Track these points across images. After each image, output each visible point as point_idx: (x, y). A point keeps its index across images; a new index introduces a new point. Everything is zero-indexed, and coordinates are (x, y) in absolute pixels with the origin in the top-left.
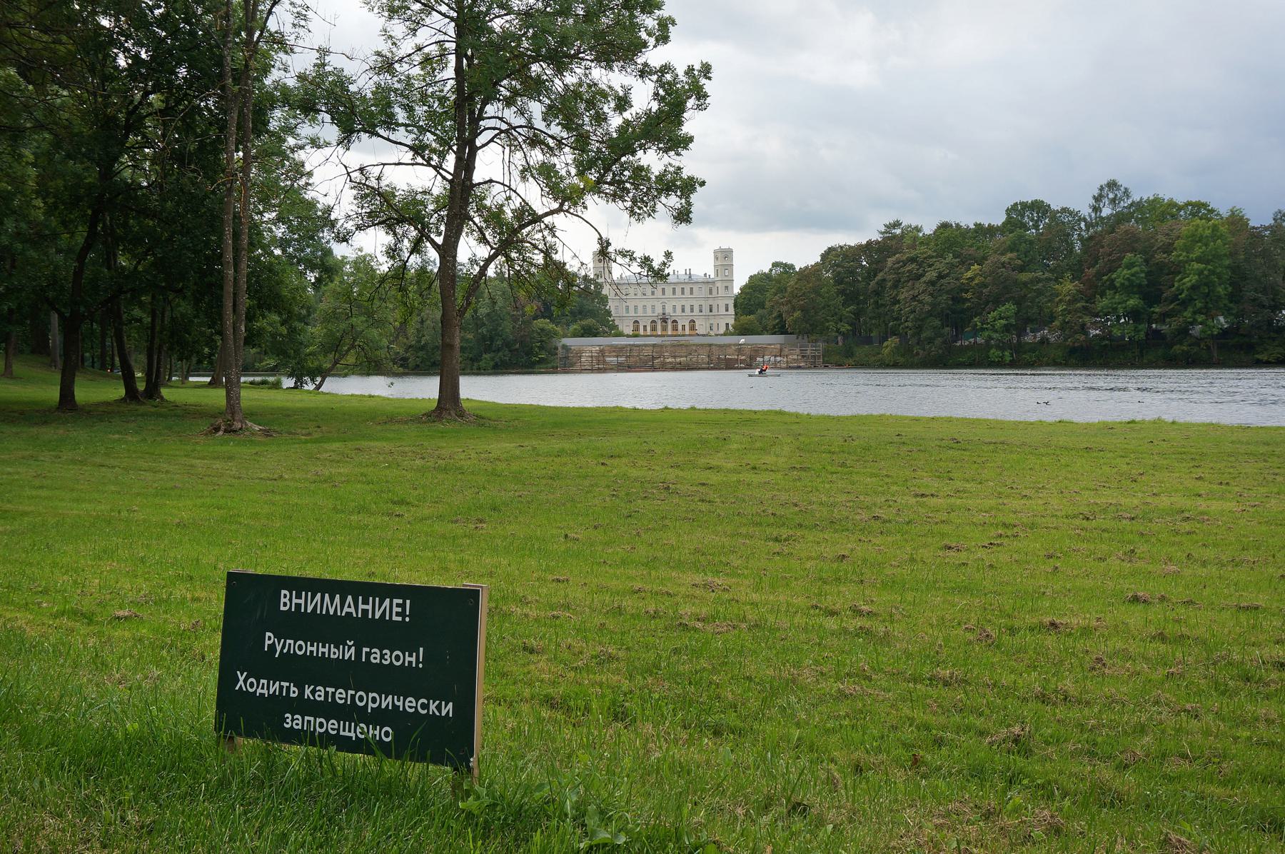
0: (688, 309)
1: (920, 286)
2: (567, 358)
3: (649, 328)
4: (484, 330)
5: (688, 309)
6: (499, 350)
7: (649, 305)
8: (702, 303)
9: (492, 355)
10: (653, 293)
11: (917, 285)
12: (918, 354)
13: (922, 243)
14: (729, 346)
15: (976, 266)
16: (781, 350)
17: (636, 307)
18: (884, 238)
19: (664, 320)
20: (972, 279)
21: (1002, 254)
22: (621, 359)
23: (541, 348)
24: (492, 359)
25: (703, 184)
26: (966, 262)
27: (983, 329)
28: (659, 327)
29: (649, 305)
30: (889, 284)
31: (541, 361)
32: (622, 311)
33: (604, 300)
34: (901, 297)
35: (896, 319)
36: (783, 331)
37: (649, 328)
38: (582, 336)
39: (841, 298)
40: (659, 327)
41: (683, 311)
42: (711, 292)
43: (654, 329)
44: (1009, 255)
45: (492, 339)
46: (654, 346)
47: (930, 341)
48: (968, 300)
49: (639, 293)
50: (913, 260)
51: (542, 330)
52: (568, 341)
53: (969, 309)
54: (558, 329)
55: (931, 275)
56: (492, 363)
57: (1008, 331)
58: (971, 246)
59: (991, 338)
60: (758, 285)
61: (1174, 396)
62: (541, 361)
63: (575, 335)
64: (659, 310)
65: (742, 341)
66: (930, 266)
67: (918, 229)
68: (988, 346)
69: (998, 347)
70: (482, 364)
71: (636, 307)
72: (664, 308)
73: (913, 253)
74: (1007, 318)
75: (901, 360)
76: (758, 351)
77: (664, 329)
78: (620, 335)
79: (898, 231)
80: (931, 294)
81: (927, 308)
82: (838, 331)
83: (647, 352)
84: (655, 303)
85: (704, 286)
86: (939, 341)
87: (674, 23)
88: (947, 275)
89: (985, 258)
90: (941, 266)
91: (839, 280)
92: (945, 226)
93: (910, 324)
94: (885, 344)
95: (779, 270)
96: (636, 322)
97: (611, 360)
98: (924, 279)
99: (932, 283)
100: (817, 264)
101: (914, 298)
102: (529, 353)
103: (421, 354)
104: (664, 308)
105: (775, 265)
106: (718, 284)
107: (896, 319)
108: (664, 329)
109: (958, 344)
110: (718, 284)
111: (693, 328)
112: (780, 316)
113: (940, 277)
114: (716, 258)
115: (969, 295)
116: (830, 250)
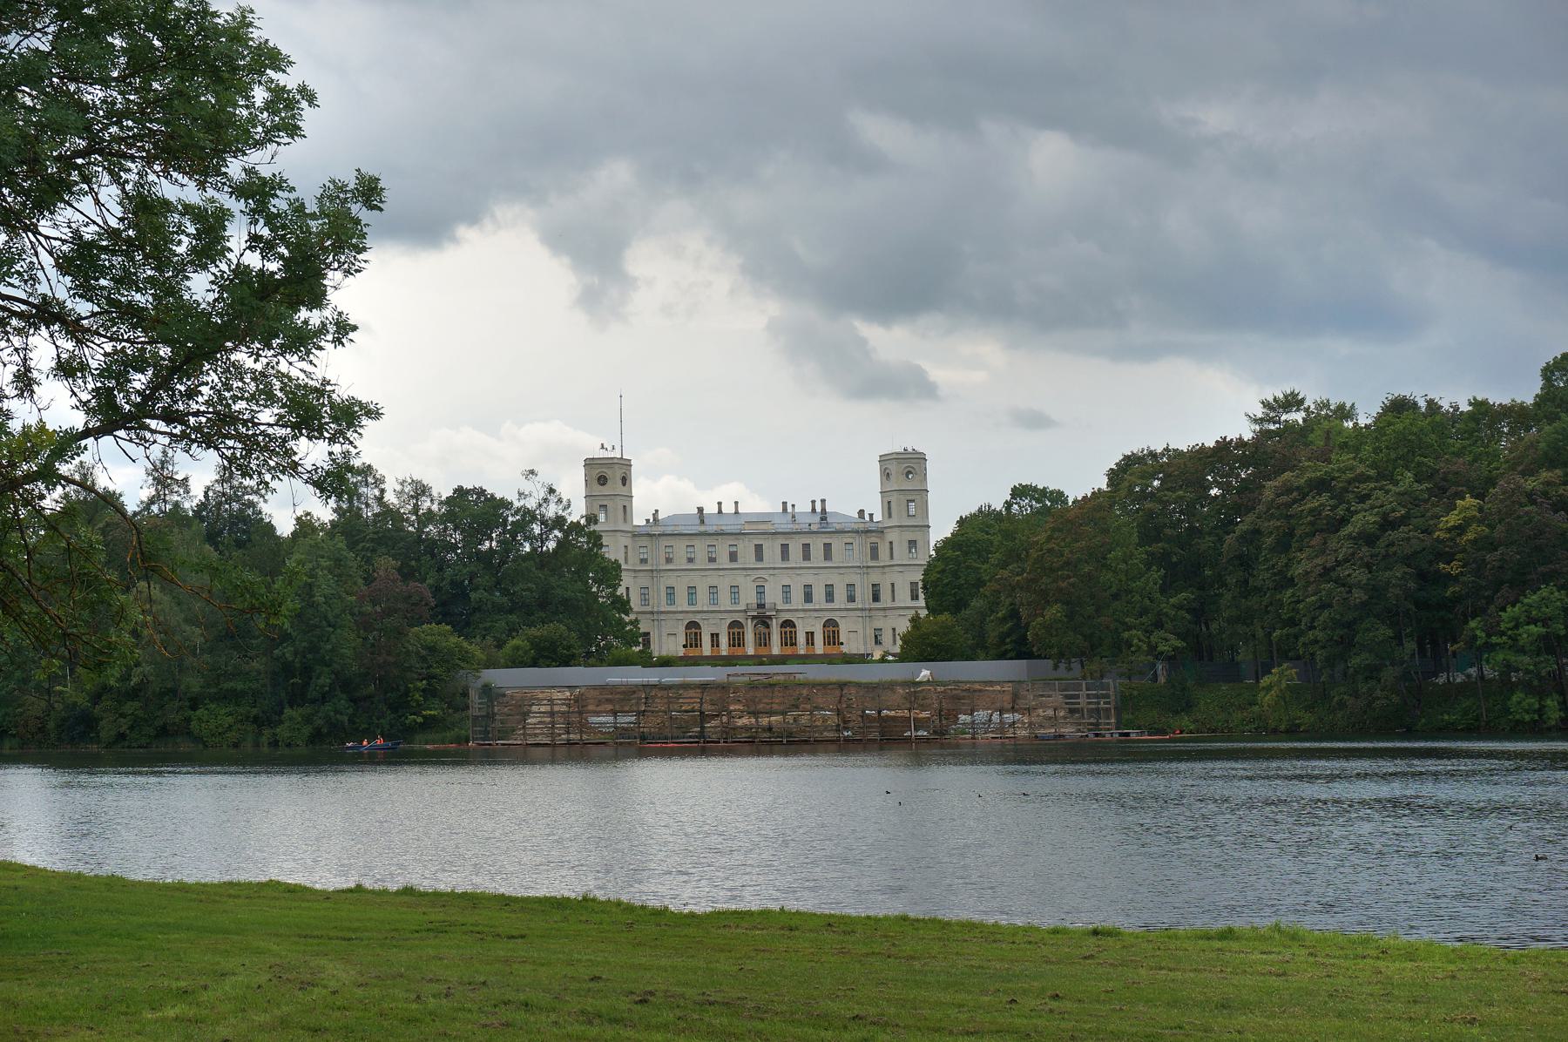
0: (819, 594)
1: (1340, 546)
2: (490, 716)
3: (724, 640)
4: (287, 651)
5: (819, 594)
6: (324, 698)
7: (724, 585)
8: (854, 578)
9: (307, 709)
10: (733, 557)
11: (1333, 544)
12: (1342, 705)
13: (1344, 446)
14: (891, 686)
15: (1469, 501)
16: (1015, 697)
17: (692, 590)
18: (1264, 435)
19: (763, 621)
20: (1460, 529)
21: (1529, 472)
22: (626, 720)
23: (429, 693)
24: (308, 720)
25: (374, 413)
26: (1445, 490)
27: (1490, 647)
28: (749, 637)
29: (724, 585)
30: (1269, 541)
31: (429, 724)
32: (663, 607)
33: (611, 573)
34: (1298, 570)
35: (1292, 622)
36: (1022, 651)
37: (724, 640)
38: (534, 664)
39: (1156, 574)
40: (749, 637)
41: (808, 597)
42: (874, 553)
43: (737, 640)
44: (1545, 475)
45: (307, 671)
46: (704, 687)
47: (1372, 672)
48: (1455, 579)
49: (724, 561)
50: (1321, 485)
51: (432, 649)
52: (501, 677)
53: (1457, 599)
54: (475, 649)
55: (1365, 519)
56: (307, 730)
57: (1550, 650)
58: (1458, 454)
59: (1509, 667)
60: (978, 532)
61: (357, 924)
62: (429, 724)
63: (515, 663)
64: (749, 597)
65: (925, 674)
66: (1363, 498)
67: (1344, 412)
68: (1506, 686)
69: (1528, 688)
70: (282, 731)
71: (692, 590)
72: (760, 591)
73: (1322, 470)
74: (1545, 622)
75: (1307, 718)
76: (961, 698)
77: (763, 640)
78: (646, 660)
79: (1298, 417)
80: (1368, 566)
81: (1359, 595)
82: (1152, 648)
83: (690, 701)
84: (740, 579)
85: (857, 541)
86: (1389, 674)
87: (311, 98)
88: (1404, 520)
89: (1492, 482)
90: (1387, 499)
91: (1151, 531)
92: (1399, 407)
93: (1320, 635)
94: (1265, 681)
95: (1026, 506)
96: (693, 625)
97: (602, 720)
98: (1348, 529)
99: (1369, 539)
100: (1097, 494)
101: (1326, 572)
102: (400, 704)
103: (130, 707)
104: (760, 591)
105: (1019, 492)
106: (892, 536)
107: (1292, 622)
108: (763, 640)
109: (1441, 680)
110: (892, 536)
111: (832, 637)
112: (1014, 614)
113: (1387, 524)
114: (886, 475)
115: (1454, 568)
116: (1130, 461)
